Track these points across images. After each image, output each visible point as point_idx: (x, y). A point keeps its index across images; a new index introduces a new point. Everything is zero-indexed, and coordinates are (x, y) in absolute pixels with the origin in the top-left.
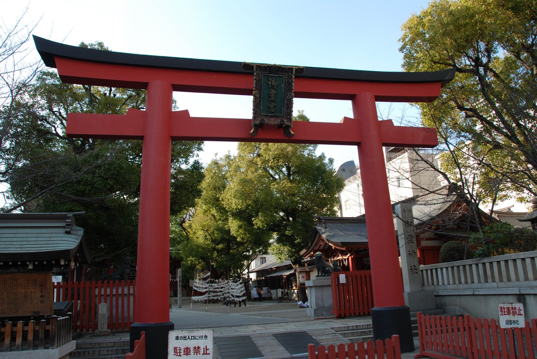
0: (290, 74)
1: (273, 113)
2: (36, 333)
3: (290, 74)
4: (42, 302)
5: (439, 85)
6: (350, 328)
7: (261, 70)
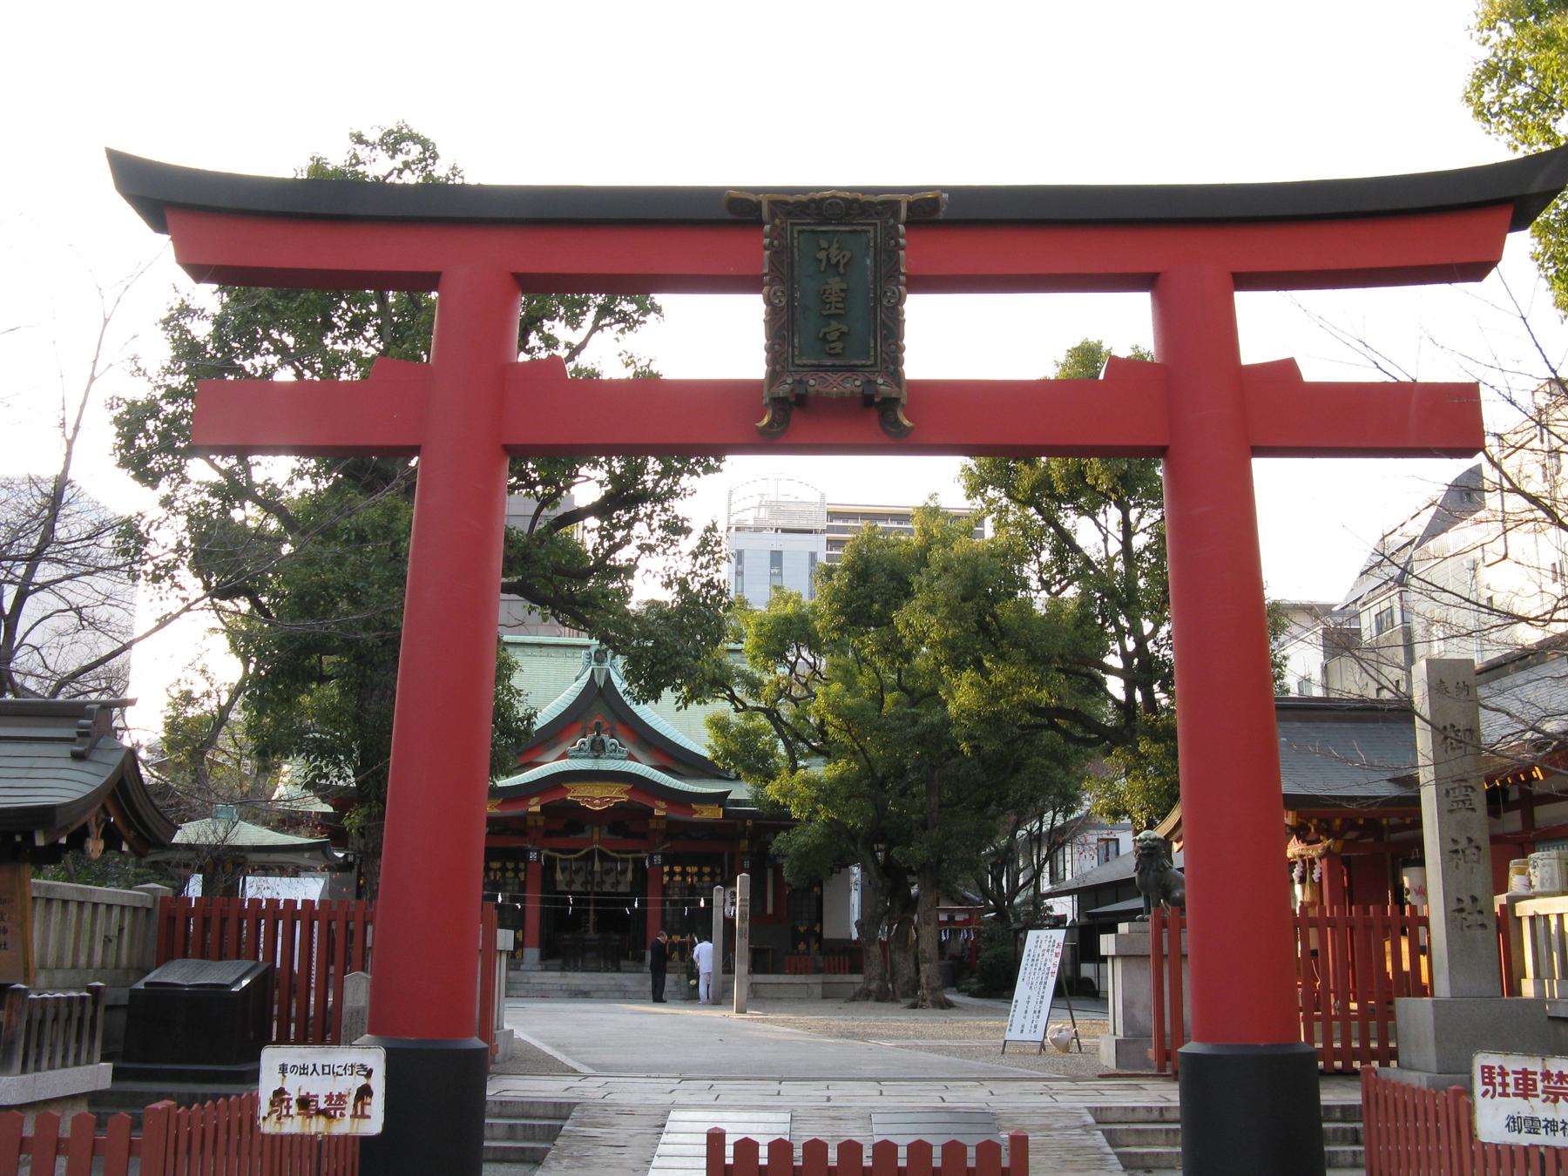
1: (837, 355)
5: (1506, 215)
6: (1167, 1116)
7: (789, 214)
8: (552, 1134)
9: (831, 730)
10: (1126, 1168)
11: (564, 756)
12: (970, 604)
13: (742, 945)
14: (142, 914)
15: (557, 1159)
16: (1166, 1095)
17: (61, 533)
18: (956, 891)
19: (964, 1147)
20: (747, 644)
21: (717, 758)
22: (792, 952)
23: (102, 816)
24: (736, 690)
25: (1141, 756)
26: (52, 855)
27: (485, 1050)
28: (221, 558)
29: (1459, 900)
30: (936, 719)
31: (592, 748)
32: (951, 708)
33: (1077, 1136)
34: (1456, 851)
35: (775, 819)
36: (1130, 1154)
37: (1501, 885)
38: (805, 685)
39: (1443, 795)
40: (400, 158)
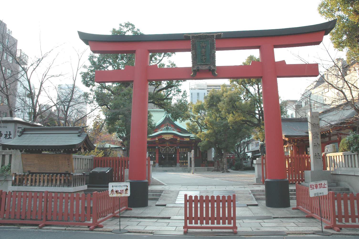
0: (213, 39)
2: (64, 180)
3: (213, 39)
4: (69, 167)
5: (324, 32)
8: (160, 195)
9: (207, 125)
10: (256, 200)
11: (161, 130)
12: (231, 103)
13: (193, 162)
14: (91, 160)
15: (160, 199)
16: (263, 187)
17: (74, 97)
18: (230, 152)
19: (225, 196)
20: (193, 110)
21: (188, 130)
22: (202, 163)
23: (83, 145)
24: (191, 118)
25: (262, 128)
26: (75, 152)
27: (148, 182)
28: (101, 99)
29: (315, 154)
30: (226, 122)
31: (166, 129)
32: (229, 121)
33: (248, 195)
34: (315, 145)
35: (198, 140)
36: (257, 198)
37: (323, 151)
38: (203, 117)
39: (313, 135)
40: (128, 28)
